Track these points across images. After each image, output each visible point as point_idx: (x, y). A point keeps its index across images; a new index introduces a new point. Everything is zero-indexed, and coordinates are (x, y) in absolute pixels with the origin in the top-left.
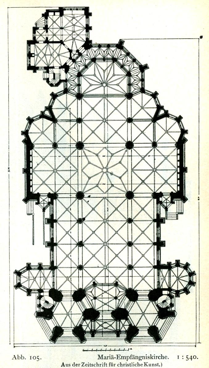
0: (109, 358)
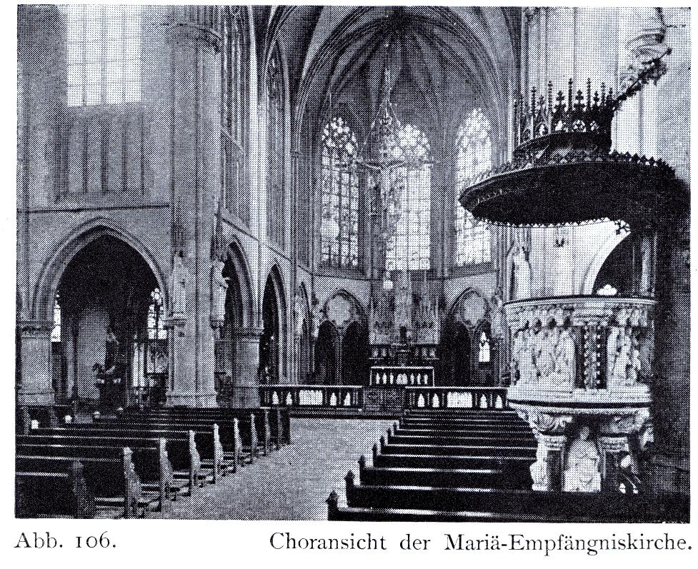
0: (483, 545)
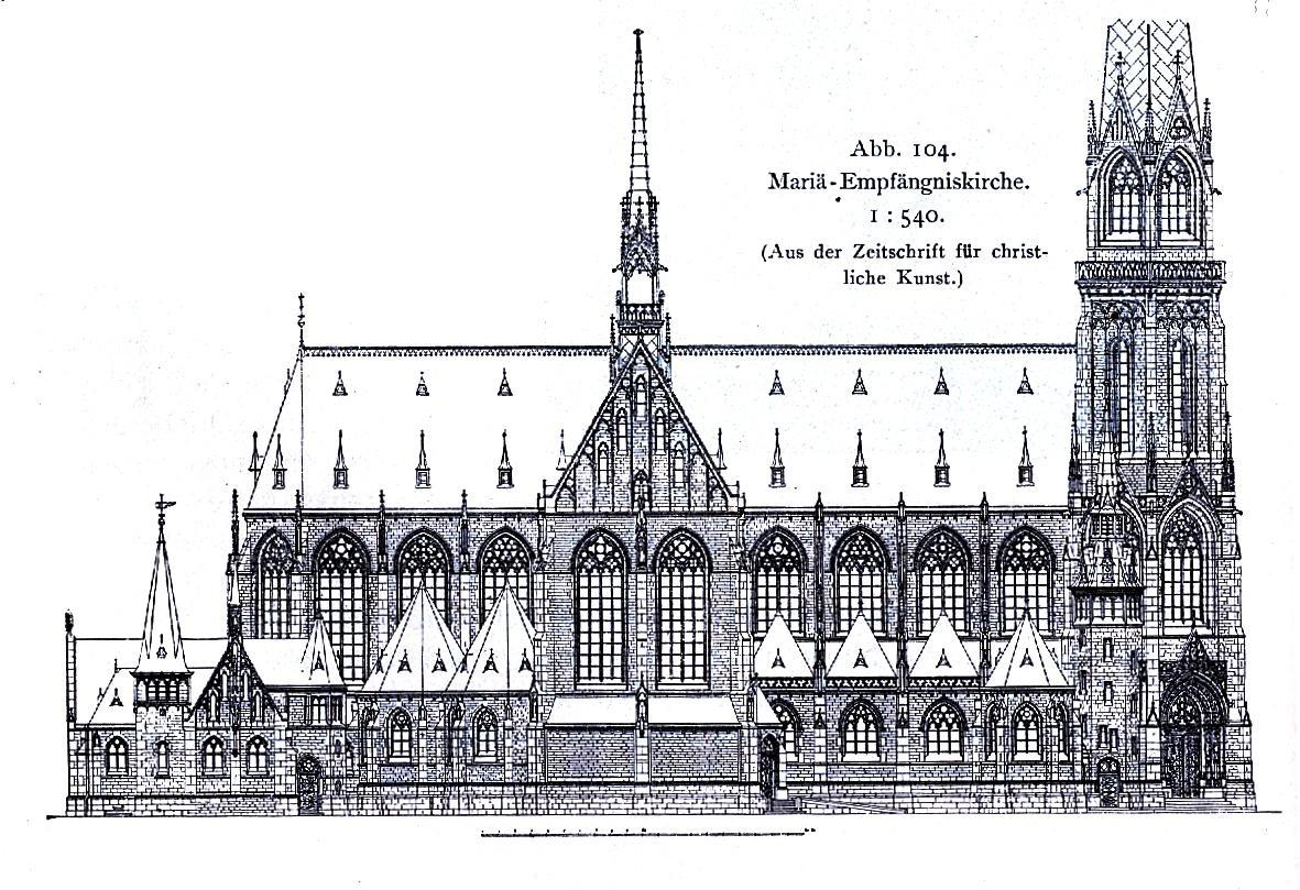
0: (808, 184)
